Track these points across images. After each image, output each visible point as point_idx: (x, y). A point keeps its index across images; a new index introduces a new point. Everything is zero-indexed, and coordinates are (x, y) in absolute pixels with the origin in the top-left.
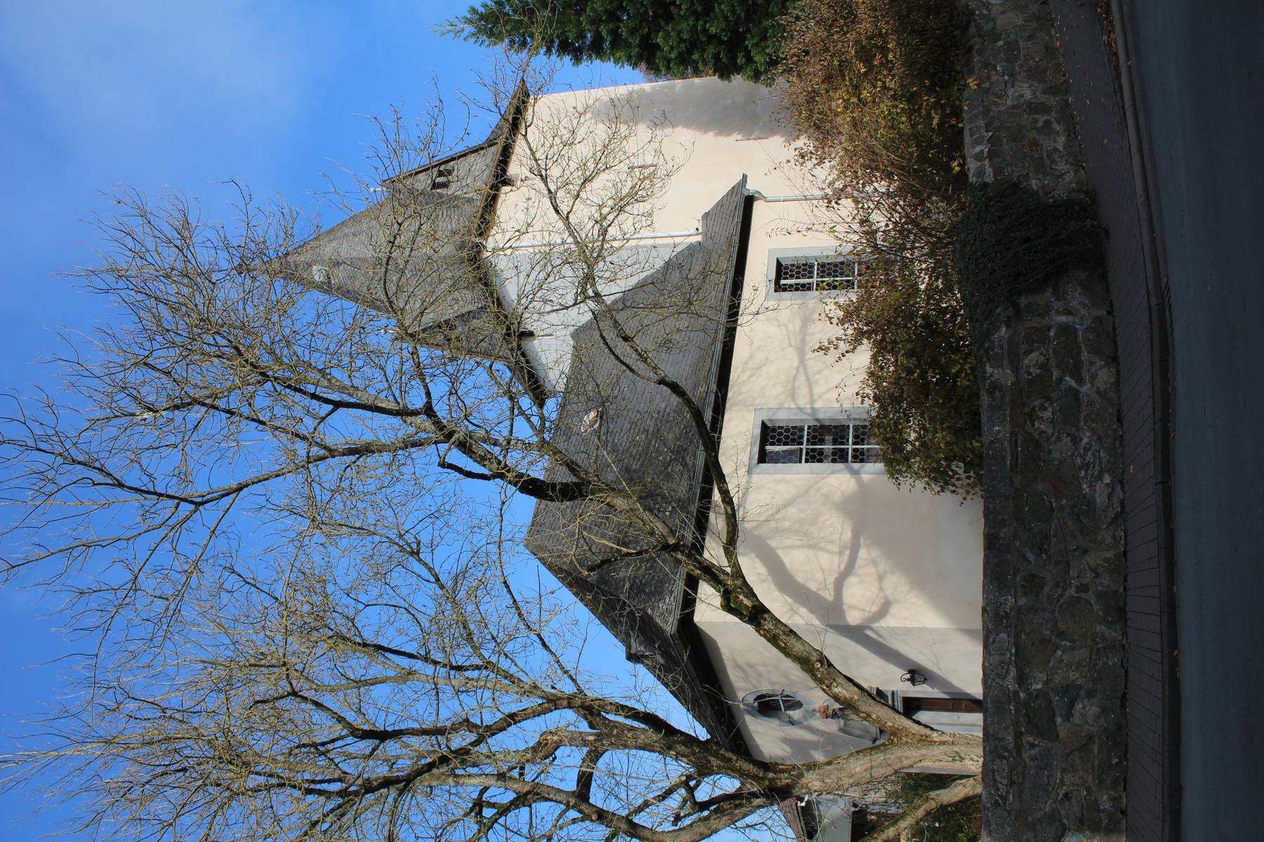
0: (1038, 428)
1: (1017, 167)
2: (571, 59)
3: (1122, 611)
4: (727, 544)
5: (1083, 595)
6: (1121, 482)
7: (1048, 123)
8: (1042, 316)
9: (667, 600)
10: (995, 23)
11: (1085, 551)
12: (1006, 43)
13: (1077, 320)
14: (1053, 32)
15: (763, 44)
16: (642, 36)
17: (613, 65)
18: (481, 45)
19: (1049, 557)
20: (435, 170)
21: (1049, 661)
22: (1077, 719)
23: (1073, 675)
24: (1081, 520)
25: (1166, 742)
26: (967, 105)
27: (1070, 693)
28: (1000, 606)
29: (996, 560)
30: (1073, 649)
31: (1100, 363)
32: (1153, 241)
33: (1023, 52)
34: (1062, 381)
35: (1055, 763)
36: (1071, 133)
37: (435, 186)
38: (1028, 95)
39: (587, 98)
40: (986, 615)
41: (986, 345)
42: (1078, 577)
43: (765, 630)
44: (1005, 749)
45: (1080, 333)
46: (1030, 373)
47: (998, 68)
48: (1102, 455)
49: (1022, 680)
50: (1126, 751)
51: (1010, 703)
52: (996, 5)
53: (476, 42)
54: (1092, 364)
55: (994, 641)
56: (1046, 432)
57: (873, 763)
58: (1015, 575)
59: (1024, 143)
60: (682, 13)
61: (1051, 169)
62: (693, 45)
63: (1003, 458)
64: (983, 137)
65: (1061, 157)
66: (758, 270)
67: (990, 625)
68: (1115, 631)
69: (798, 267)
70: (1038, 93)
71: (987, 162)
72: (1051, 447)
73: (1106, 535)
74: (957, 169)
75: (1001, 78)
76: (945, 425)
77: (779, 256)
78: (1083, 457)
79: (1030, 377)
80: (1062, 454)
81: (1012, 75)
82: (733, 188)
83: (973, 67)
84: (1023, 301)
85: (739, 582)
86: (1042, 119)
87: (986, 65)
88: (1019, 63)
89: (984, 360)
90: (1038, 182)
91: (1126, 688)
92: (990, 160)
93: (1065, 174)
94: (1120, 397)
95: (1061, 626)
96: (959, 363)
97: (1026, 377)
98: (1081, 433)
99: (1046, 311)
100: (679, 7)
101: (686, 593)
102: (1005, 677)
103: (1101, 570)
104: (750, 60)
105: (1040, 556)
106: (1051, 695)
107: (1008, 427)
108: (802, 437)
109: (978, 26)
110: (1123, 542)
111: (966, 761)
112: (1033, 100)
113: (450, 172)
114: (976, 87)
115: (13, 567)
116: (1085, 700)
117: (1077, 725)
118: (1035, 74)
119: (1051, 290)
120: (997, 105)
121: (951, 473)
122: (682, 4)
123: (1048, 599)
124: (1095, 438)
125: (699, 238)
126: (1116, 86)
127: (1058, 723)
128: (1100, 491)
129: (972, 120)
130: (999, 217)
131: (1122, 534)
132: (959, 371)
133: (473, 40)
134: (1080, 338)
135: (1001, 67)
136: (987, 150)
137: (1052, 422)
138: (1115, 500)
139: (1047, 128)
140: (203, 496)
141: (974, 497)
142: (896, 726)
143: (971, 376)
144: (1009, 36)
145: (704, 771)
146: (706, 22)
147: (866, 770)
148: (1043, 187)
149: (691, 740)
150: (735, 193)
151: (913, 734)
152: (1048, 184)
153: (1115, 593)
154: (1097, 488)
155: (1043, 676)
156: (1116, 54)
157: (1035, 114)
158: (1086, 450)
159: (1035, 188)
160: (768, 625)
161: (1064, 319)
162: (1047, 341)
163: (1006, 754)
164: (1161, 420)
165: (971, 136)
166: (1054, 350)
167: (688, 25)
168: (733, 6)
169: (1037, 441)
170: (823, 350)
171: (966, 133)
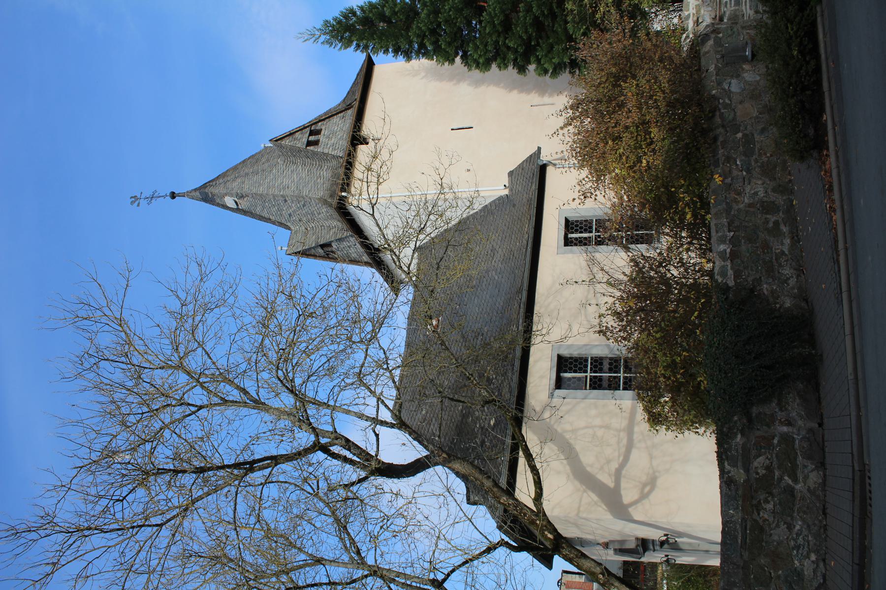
0: (763, 517)
1: (752, 270)
6: (824, 560)
7: (776, 223)
8: (768, 426)
12: (745, 135)
13: (795, 431)
15: (550, 56)
18: (334, 48)
20: (308, 130)
24: (793, 587)
32: (859, 417)
33: (758, 146)
34: (781, 480)
36: (795, 238)
37: (309, 143)
45: (797, 441)
46: (757, 473)
47: (738, 163)
48: (810, 538)
54: (805, 466)
56: (768, 520)
61: (779, 272)
63: (736, 538)
64: (727, 237)
69: (581, 223)
70: (769, 191)
71: (729, 263)
75: (740, 173)
78: (795, 540)
79: (758, 476)
80: (779, 537)
81: (748, 171)
82: (531, 156)
83: (718, 159)
84: (755, 411)
86: (772, 218)
87: (728, 159)
90: (768, 287)
92: (731, 261)
97: (754, 475)
98: (794, 522)
107: (740, 514)
109: (722, 115)
112: (765, 199)
113: (318, 132)
114: (721, 183)
120: (737, 202)
125: (506, 192)
130: (738, 326)
134: (797, 446)
135: (741, 161)
136: (728, 250)
137: (773, 512)
138: (819, 574)
139: (775, 231)
144: (746, 128)
146: (506, 38)
148: (772, 292)
154: (806, 564)
157: (766, 213)
158: (798, 535)
159: (766, 292)
161: (785, 429)
162: (772, 448)
165: (717, 232)
166: (777, 456)
168: (526, 29)
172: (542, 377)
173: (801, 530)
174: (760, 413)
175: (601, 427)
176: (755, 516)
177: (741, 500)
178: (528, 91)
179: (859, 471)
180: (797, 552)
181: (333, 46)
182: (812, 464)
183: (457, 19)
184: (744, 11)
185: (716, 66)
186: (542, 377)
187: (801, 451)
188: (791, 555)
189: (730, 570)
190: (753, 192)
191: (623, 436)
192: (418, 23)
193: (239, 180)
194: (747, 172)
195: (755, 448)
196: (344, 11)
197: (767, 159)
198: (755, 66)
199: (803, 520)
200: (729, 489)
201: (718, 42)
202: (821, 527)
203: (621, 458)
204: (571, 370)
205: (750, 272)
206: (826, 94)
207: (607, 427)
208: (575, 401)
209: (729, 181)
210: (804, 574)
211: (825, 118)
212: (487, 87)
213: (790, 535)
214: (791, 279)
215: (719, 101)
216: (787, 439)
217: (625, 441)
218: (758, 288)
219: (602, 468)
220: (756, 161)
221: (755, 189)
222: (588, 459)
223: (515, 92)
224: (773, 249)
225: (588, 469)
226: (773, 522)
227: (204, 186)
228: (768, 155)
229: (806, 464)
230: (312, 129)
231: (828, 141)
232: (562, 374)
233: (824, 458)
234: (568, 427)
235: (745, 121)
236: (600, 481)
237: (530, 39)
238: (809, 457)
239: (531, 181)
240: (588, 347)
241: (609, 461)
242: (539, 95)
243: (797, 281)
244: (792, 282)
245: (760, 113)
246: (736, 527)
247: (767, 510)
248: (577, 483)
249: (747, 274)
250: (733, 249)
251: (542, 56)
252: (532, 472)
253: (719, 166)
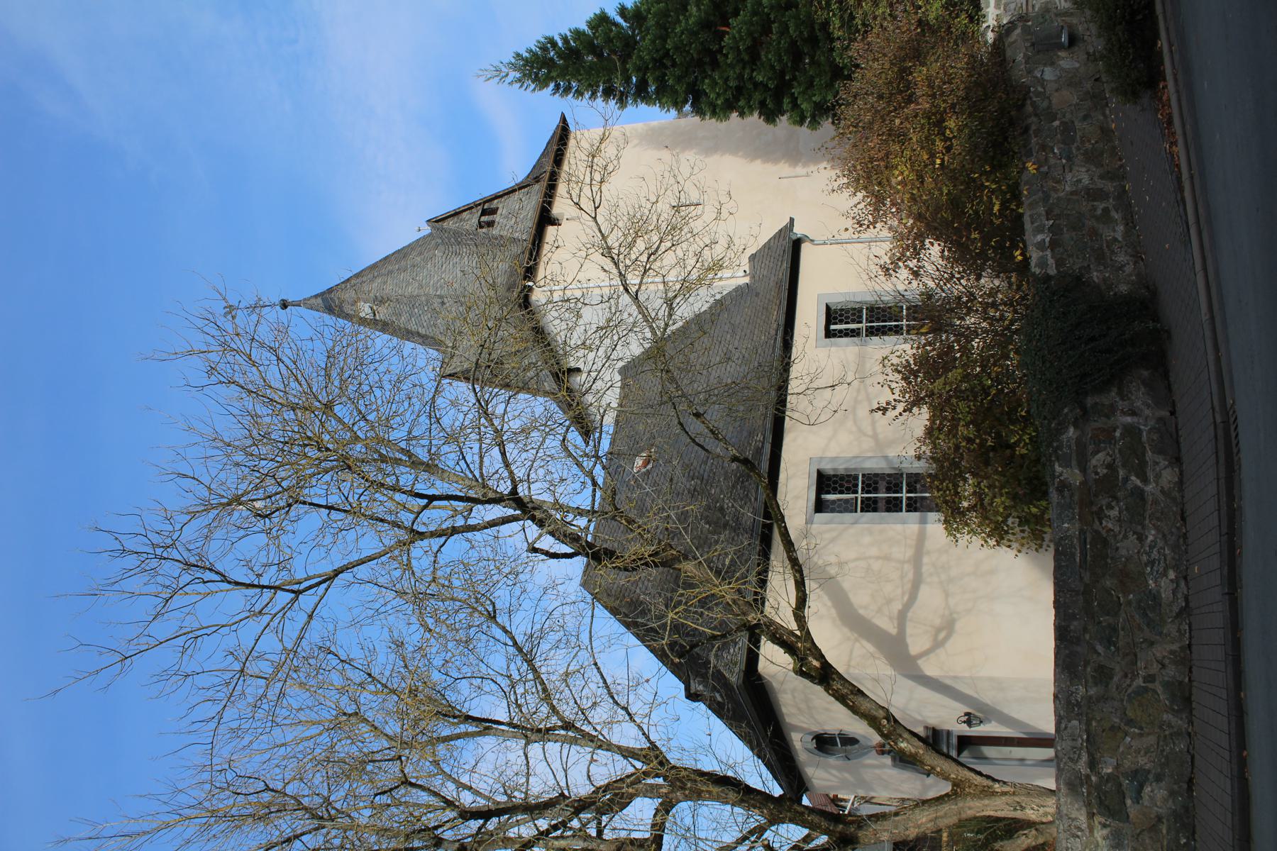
0: (1106, 526)
1: (1078, 258)
2: (616, 103)
3: (1188, 700)
4: (796, 609)
5: (1150, 685)
6: (1185, 578)
7: (1106, 210)
8: (1108, 417)
9: (732, 651)
10: (1050, 101)
11: (1152, 644)
14: (1108, 112)
16: (688, 84)
17: (659, 109)
19: (1118, 649)
21: (1119, 747)
22: (1146, 800)
23: (1143, 761)
25: (1237, 837)
26: (1027, 190)
27: (1139, 777)
28: (1071, 695)
29: (1067, 652)
30: (1141, 735)
31: (1164, 463)
33: (1079, 134)
35: (1126, 842)
36: (1130, 223)
38: (1086, 181)
39: (659, 187)
40: (1058, 702)
41: (1055, 444)
42: (1145, 668)
43: (833, 690)
44: (1079, 829)
46: (1097, 473)
47: (1056, 151)
48: (1167, 552)
49: (1093, 764)
50: (1194, 833)
51: (1082, 785)
52: (1051, 81)
53: (521, 86)
54: (1157, 463)
55: (1066, 728)
56: (1113, 530)
57: (938, 814)
58: (1085, 666)
59: (1084, 232)
60: (729, 61)
61: (1111, 260)
62: (739, 90)
63: (1073, 555)
64: (1045, 225)
65: (1121, 248)
66: (809, 318)
67: (1062, 713)
68: (1181, 719)
70: (1096, 179)
71: (1049, 253)
72: (1118, 545)
73: (1171, 628)
74: (1020, 258)
75: (1058, 161)
76: (1003, 491)
77: (830, 300)
78: (1148, 554)
80: (1128, 551)
81: (1069, 159)
82: (781, 231)
83: (1031, 149)
84: (1089, 401)
85: (808, 645)
86: (1100, 206)
87: (1043, 147)
88: (1075, 145)
89: (1053, 459)
91: (1192, 773)
92: (1052, 250)
93: (1125, 266)
94: (1183, 497)
95: (1130, 714)
96: (1018, 434)
97: (1094, 476)
99: (1112, 409)
100: (726, 56)
101: (750, 650)
102: (1077, 761)
103: (1166, 661)
104: (795, 105)
105: (1108, 648)
106: (1121, 779)
107: (1077, 525)
108: (857, 485)
109: (1033, 104)
110: (1187, 635)
111: (1027, 811)
112: (1091, 186)
113: (494, 211)
114: (1035, 171)
115: (126, 658)
116: (1154, 784)
117: (1146, 807)
118: (1092, 158)
119: (1115, 390)
120: (1056, 190)
121: (1006, 528)
122: (729, 53)
123: (1117, 688)
124: (1160, 536)
125: (747, 280)
126: (1179, 198)
127: (1128, 805)
128: (1164, 585)
129: (1031, 206)
130: (1063, 313)
131: (1187, 627)
132: (1019, 441)
133: (519, 85)
134: (1144, 438)
135: (1058, 149)
136: (1048, 240)
137: (1119, 520)
138: (1180, 595)
139: (1106, 217)
140: (300, 583)
141: (1029, 551)
142: (959, 778)
143: (1029, 446)
144: (1064, 116)
145: (774, 821)
146: (753, 70)
147: (931, 821)
148: (1105, 280)
149: (766, 798)
150: (782, 235)
151: (976, 785)
152: (1109, 277)
153: (1181, 683)
154: (1163, 584)
155: (1114, 761)
156: (1178, 166)
157: (1093, 201)
158: (1151, 547)
160: (836, 685)
161: (1129, 419)
162: (1113, 442)
163: (1079, 833)
164: (1227, 533)
165: (1032, 223)
166: (1120, 451)
167: (735, 73)
168: (780, 56)
169: (1105, 539)
170: (880, 410)
171: (1027, 219)
172: (797, 498)
173: (1154, 543)
174: (1096, 404)
175: (878, 558)
176: (1096, 525)
177: (1077, 507)
178: (776, 161)
179: (1223, 422)
180: (1152, 568)
181: (524, 88)
182: (1164, 460)
183: (691, 44)
186: (797, 498)
187: (1150, 445)
188: (1144, 573)
189: (1067, 601)
191: (908, 568)
192: (640, 51)
193: (379, 280)
195: (1092, 442)
196: (543, 40)
197: (1091, 146)
198: (1072, 53)
199: (1157, 528)
200: (1063, 496)
201: (1026, 30)
202: (1179, 537)
203: (906, 598)
204: (835, 491)
205: (1076, 260)
206: (1161, 18)
207: (887, 558)
208: (842, 527)
209: (1045, 169)
210: (1162, 598)
211: (1159, 45)
212: (722, 155)
213: (1142, 547)
214: (1127, 266)
216: (1131, 431)
217: (910, 575)
218: (1087, 276)
219: (879, 610)
220: (1078, 149)
222: (861, 599)
223: (758, 162)
225: (861, 612)
226: (1120, 533)
227: (330, 290)
229: (1158, 460)
230: (485, 207)
231: (1164, 70)
232: (823, 496)
233: (1179, 451)
236: (877, 626)
237: (783, 73)
238: (1161, 451)
239: (780, 259)
240: (858, 460)
241: (889, 601)
242: (790, 166)
243: (1134, 268)
244: (1129, 269)
245: (1081, 100)
246: (1072, 542)
247: (1112, 517)
248: (846, 630)
249: (1072, 262)
251: (799, 93)
252: (793, 567)
253: (1032, 155)
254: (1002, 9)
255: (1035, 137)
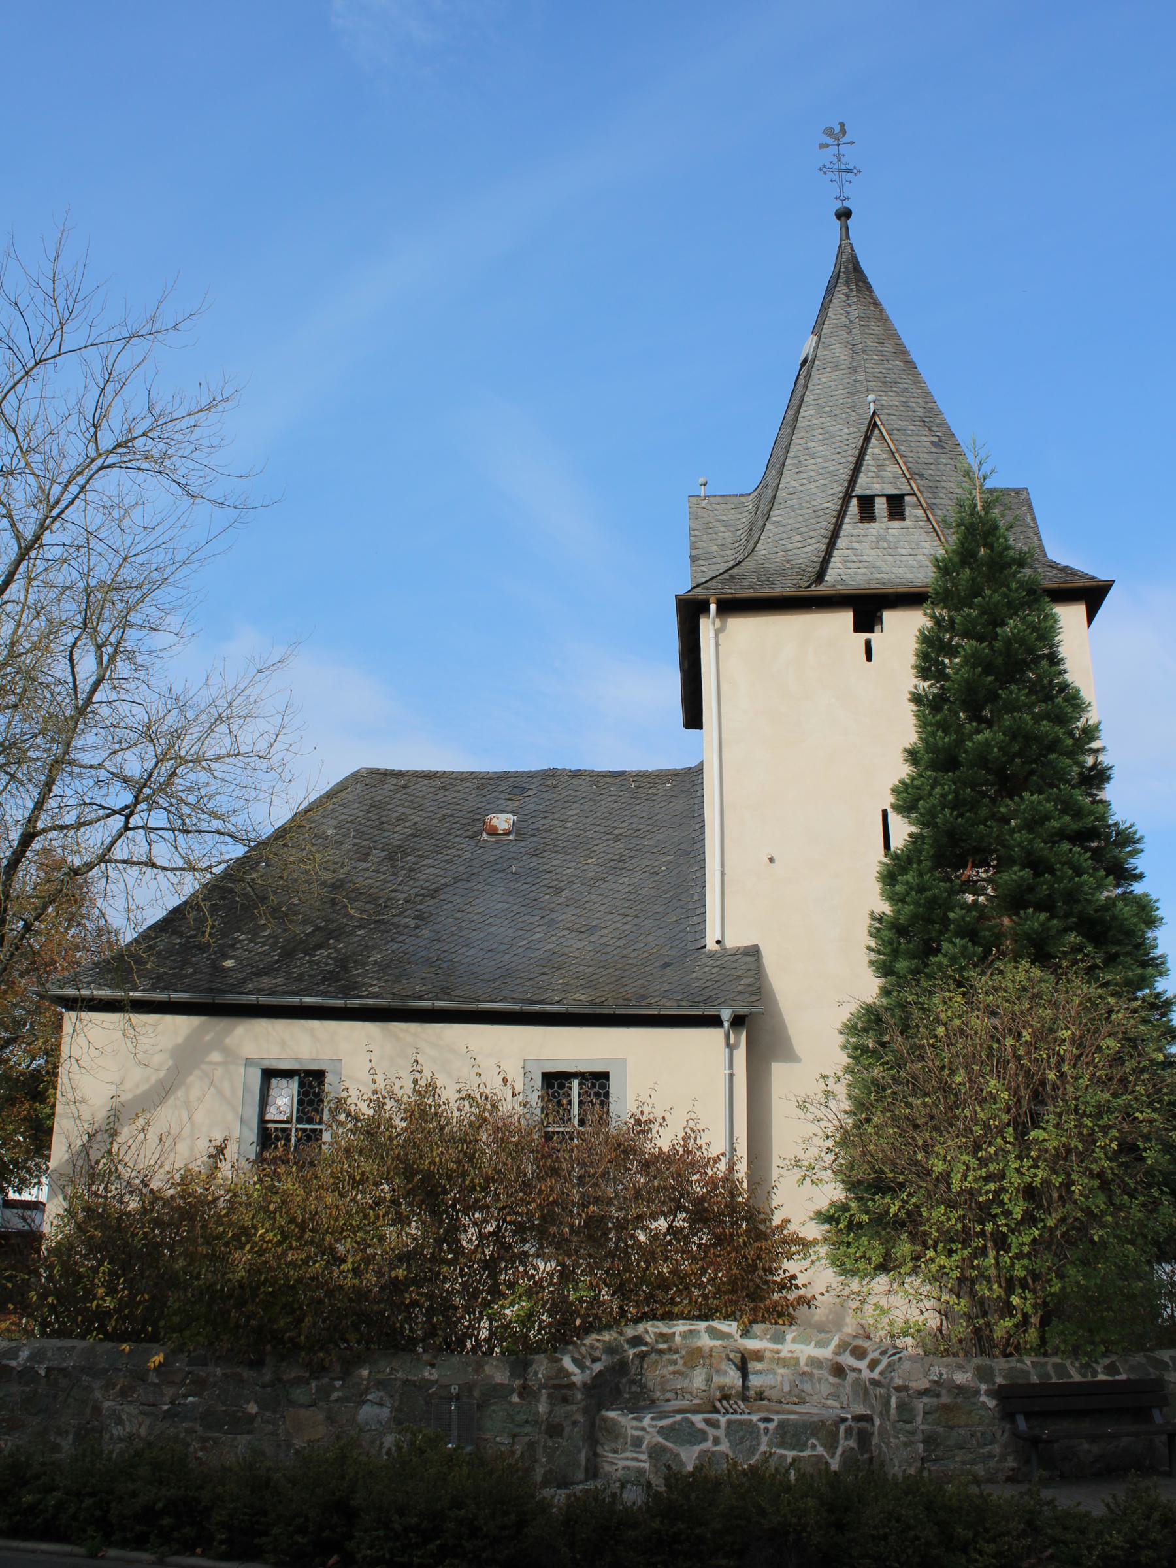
12: (252, 1418)
47: (190, 1399)
75: (167, 1399)
81: (168, 1415)
112: (107, 1436)
125: (711, 945)
136: (13, 1363)
184: (623, 1455)
185: (433, 1383)
190: (124, 1417)
194: (166, 1411)
215: (339, 1379)
221: (130, 1421)
224: (7, 1437)
228: (200, 1454)
234: (195, 1093)
235: (284, 1423)
250: (15, 1372)
254: (806, 1369)
255: (224, 1374)
